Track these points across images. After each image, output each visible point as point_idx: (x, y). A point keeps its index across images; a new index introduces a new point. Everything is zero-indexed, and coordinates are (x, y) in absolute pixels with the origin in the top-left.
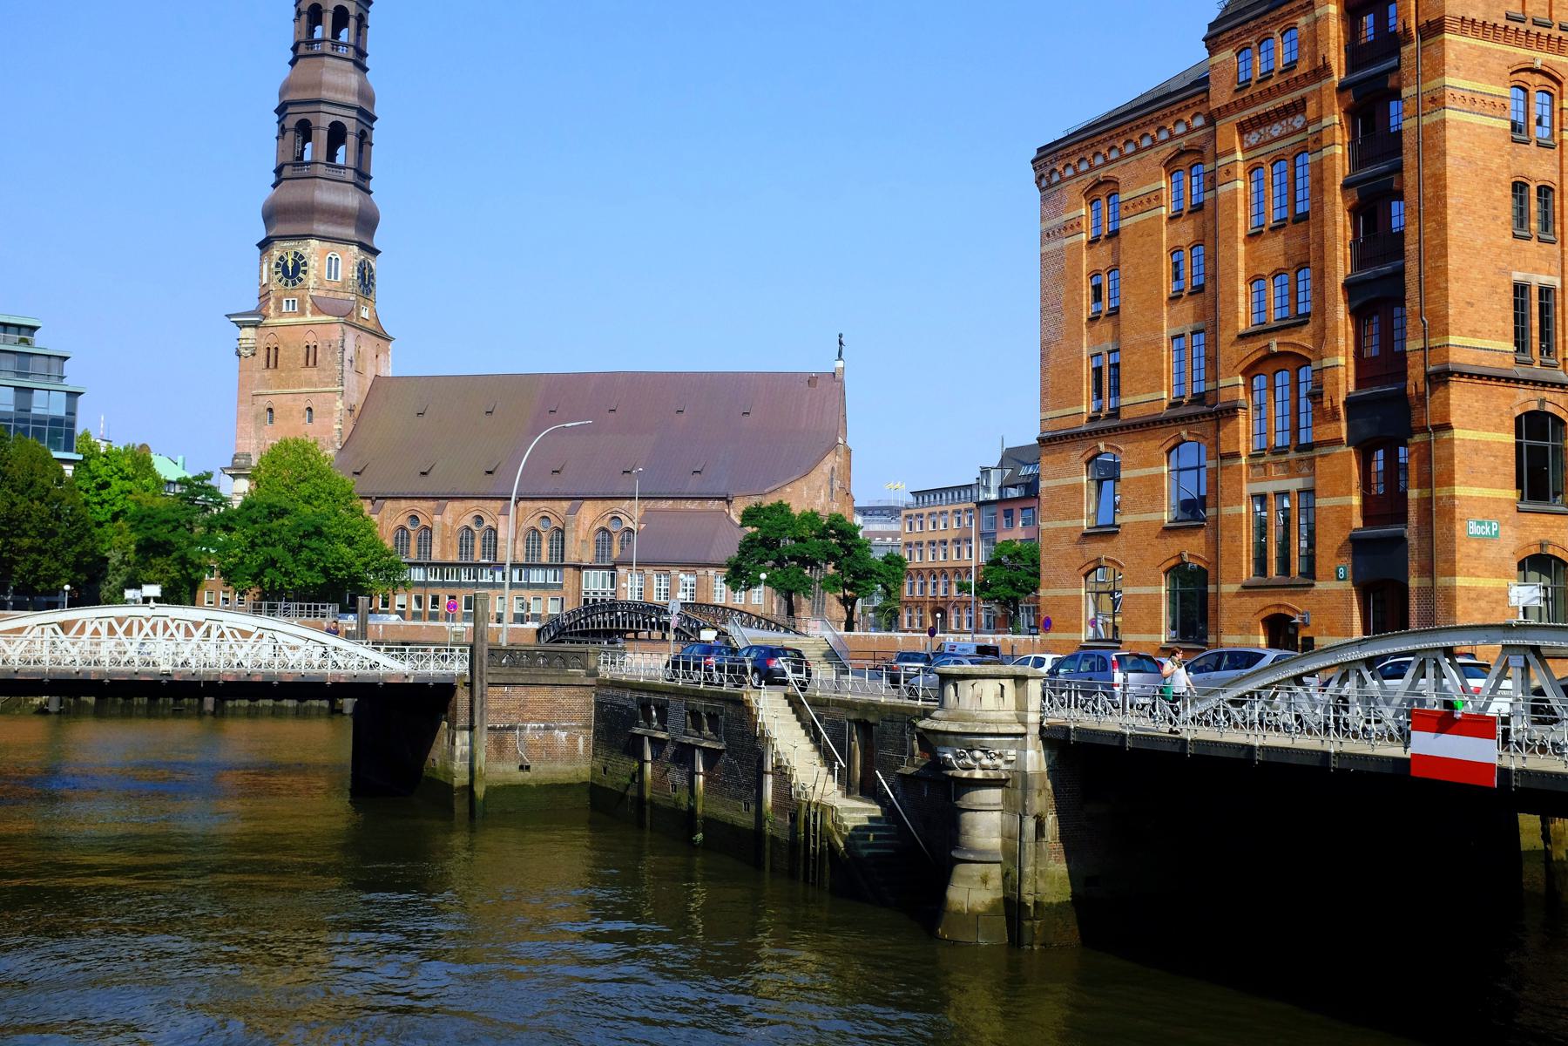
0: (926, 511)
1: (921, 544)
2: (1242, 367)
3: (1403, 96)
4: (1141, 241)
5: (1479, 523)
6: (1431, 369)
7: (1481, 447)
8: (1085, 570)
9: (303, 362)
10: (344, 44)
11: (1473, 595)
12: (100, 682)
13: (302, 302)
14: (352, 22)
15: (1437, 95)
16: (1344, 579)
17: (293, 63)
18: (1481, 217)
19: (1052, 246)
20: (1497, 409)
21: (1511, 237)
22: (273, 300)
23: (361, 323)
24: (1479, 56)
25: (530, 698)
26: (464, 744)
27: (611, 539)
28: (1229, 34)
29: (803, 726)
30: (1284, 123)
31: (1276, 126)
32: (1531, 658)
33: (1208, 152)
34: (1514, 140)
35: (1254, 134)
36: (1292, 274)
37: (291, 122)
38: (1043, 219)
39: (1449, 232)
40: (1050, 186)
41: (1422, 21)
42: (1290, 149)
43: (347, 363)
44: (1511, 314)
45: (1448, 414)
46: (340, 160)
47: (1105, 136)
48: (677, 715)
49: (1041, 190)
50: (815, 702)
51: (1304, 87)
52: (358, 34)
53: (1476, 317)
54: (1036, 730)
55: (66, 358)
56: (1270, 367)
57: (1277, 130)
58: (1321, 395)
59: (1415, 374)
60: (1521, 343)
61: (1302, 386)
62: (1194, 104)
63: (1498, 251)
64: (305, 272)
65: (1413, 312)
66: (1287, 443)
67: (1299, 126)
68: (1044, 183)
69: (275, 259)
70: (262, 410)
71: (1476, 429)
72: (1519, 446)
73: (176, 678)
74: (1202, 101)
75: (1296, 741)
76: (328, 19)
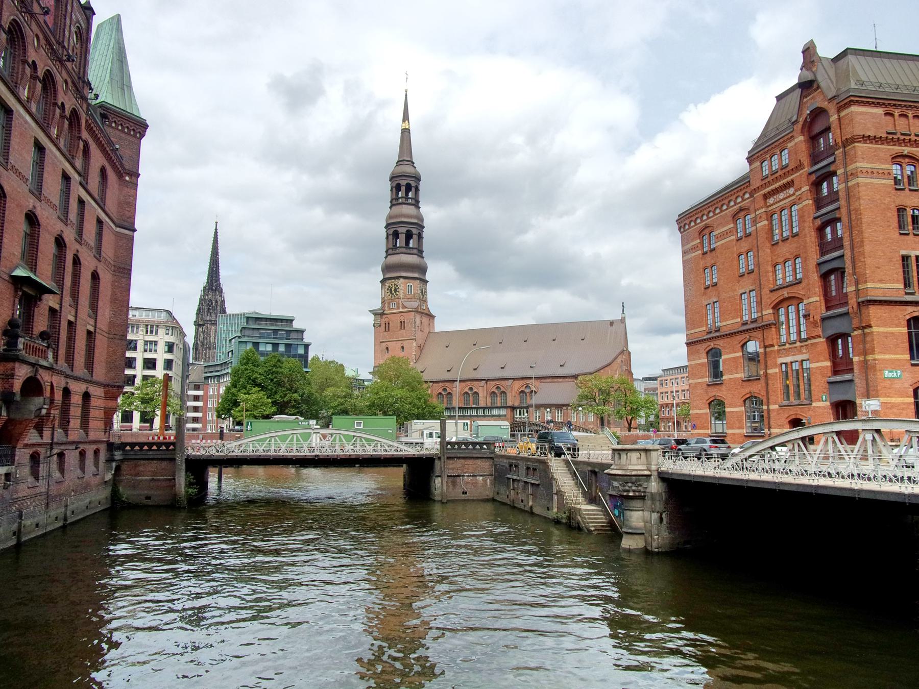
0: (669, 378)
1: (667, 393)
2: (772, 305)
3: (838, 174)
4: (725, 251)
5: (890, 372)
6: (860, 300)
7: (889, 335)
8: (708, 402)
9: (399, 328)
10: (410, 198)
11: (889, 406)
12: (292, 459)
13: (398, 304)
14: (413, 189)
15: (854, 172)
16: (826, 401)
17: (391, 207)
18: (880, 226)
19: (688, 257)
20: (896, 316)
21: (898, 234)
22: (387, 304)
23: (422, 311)
24: (874, 152)
25: (466, 463)
26: (438, 483)
27: (526, 395)
28: (757, 155)
29: (571, 473)
30: (785, 192)
31: (781, 194)
32: (876, 436)
33: (752, 209)
34: (897, 189)
35: (772, 199)
36: (793, 260)
37: (391, 231)
38: (682, 246)
39: (864, 235)
40: (685, 231)
41: (844, 138)
42: (788, 204)
43: (416, 327)
44: (901, 270)
45: (869, 320)
46: (411, 245)
47: (706, 206)
48: (522, 470)
49: (681, 233)
50: (575, 463)
51: (792, 175)
52: (416, 194)
53: (882, 273)
54: (655, 474)
55: (304, 331)
56: (786, 304)
57: (781, 196)
58: (809, 315)
59: (853, 302)
60: (907, 284)
61: (801, 312)
62: (744, 188)
63: (891, 241)
64: (399, 292)
65: (849, 274)
66: (795, 339)
67: (792, 193)
68: (682, 230)
69: (387, 287)
70: (385, 348)
71: (885, 326)
72: (910, 334)
73: (321, 457)
74: (747, 186)
75: (836, 483)
76: (403, 188)
